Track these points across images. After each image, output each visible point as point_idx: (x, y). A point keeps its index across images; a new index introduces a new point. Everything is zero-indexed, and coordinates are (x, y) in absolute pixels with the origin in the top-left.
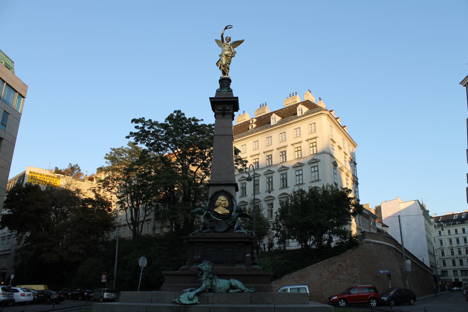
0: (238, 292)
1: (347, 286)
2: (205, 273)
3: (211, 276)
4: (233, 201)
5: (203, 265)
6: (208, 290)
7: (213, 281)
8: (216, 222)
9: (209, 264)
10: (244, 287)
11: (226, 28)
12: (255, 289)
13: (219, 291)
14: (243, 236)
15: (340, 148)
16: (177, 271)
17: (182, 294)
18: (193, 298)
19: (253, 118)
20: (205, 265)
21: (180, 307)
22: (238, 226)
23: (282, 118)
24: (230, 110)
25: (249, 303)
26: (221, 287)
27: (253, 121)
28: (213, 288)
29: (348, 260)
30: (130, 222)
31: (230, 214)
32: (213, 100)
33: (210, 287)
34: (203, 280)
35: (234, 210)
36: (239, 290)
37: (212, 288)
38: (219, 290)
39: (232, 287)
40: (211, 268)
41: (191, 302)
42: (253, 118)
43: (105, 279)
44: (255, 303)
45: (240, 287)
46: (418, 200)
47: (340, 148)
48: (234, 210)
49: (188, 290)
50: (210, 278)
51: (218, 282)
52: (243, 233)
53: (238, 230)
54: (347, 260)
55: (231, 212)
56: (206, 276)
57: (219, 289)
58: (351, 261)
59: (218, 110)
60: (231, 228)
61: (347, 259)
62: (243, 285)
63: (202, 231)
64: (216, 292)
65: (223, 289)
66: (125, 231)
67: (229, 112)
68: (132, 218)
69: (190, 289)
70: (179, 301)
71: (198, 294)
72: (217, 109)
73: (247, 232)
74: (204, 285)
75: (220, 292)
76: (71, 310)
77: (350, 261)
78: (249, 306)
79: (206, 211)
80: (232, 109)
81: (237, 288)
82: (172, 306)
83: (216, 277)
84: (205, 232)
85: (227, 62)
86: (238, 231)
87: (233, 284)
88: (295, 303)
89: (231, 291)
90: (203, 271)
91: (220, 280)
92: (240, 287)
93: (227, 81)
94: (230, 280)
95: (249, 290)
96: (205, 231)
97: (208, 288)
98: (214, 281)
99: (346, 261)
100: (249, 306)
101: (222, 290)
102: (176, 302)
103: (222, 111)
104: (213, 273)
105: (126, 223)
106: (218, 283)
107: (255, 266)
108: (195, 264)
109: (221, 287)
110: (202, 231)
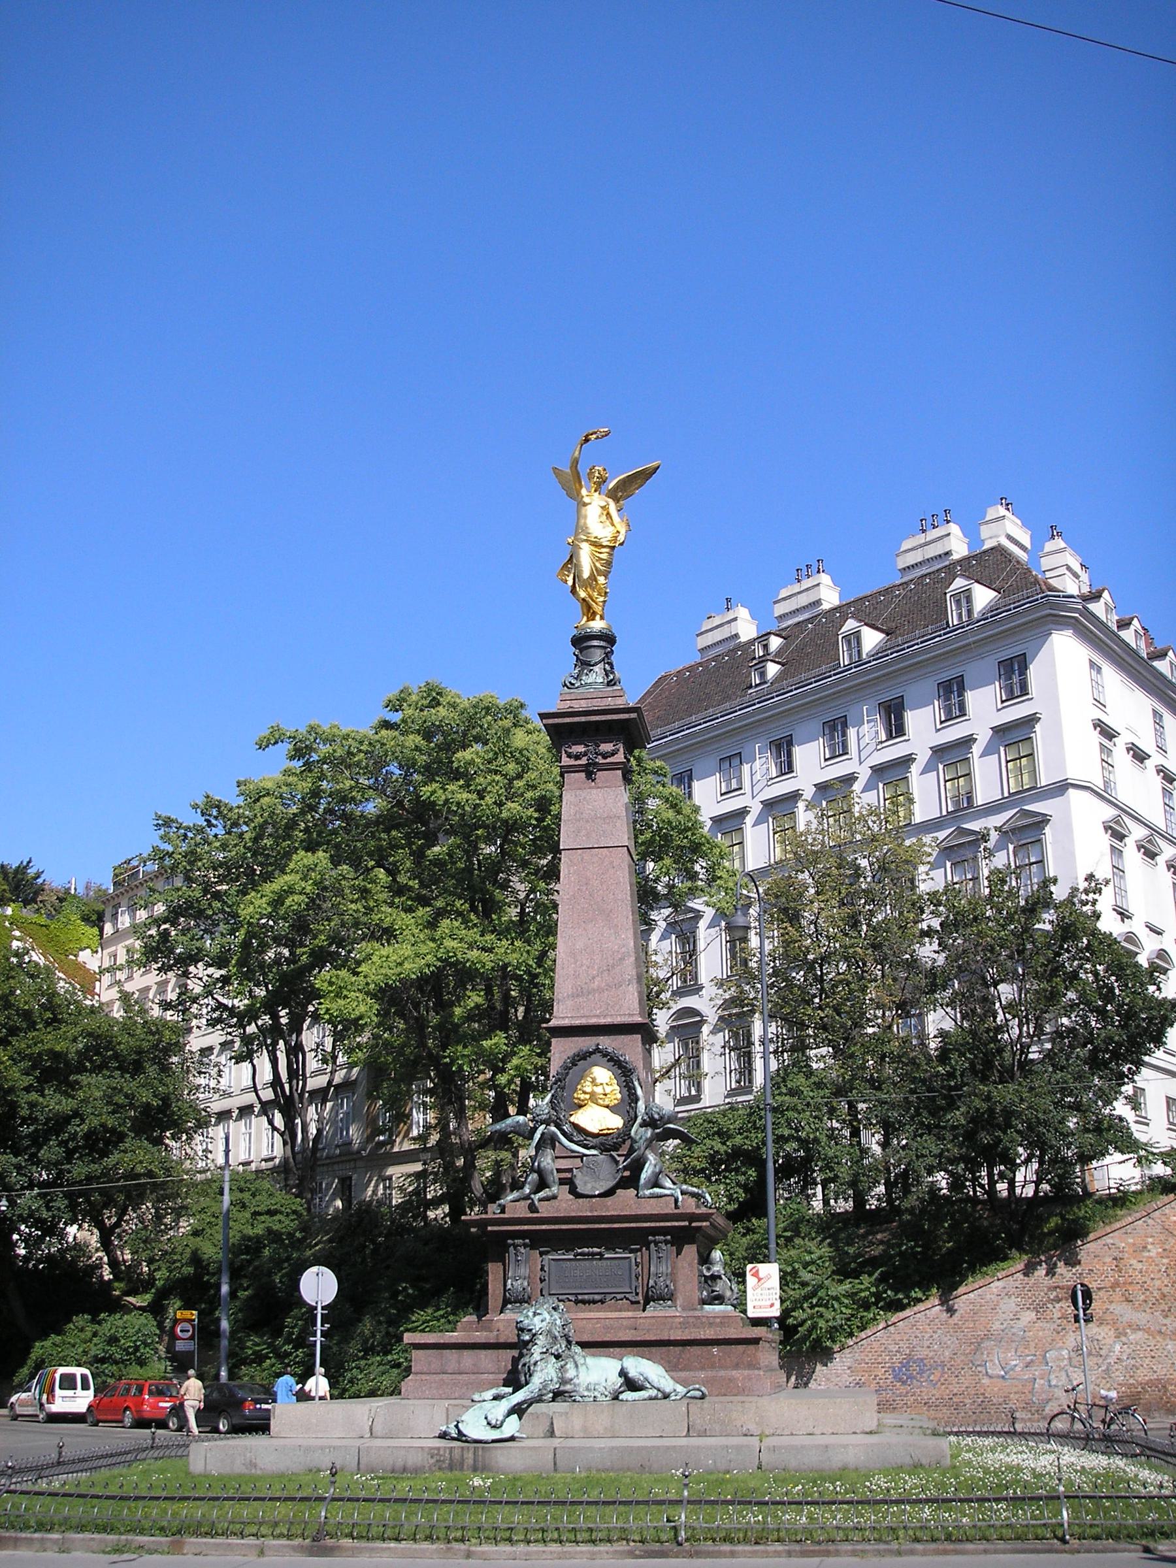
0: (651, 1398)
1: (1149, 1349)
2: (541, 1340)
3: (560, 1347)
4: (636, 1083)
5: (535, 1314)
6: (551, 1395)
7: (568, 1366)
8: (579, 1159)
9: (555, 1309)
10: (671, 1382)
11: (587, 440)
12: (703, 1389)
13: (590, 1397)
14: (670, 1209)
15: (1139, 756)
16: (451, 1334)
17: (467, 1408)
18: (502, 1423)
19: (769, 633)
20: (539, 1314)
21: (462, 1448)
22: (653, 1172)
23: (888, 634)
24: (613, 754)
25: (684, 1434)
26: (595, 1384)
27: (766, 647)
28: (568, 1387)
29: (1153, 1244)
30: (268, 1095)
31: (624, 1134)
32: (550, 721)
33: (557, 1386)
34: (535, 1364)
35: (639, 1120)
36: (653, 1393)
37: (562, 1388)
38: (586, 1393)
39: (632, 1385)
40: (558, 1322)
41: (496, 1434)
42: (769, 633)
43: (192, 1338)
44: (703, 1434)
45: (656, 1380)
46: (501, 1426)
47: (1139, 756)
48: (639, 1120)
49: (489, 1395)
50: (557, 1357)
51: (584, 1367)
52: (668, 1198)
53: (652, 1188)
54: (1149, 1247)
55: (630, 1121)
56: (544, 1350)
57: (588, 1389)
58: (1165, 1250)
59: (569, 756)
60: (630, 1181)
61: (1150, 1240)
62: (667, 1377)
63: (533, 1196)
64: (578, 1398)
65: (602, 1389)
66: (250, 1134)
67: (609, 760)
68: (276, 1083)
69: (494, 1391)
70: (460, 1432)
71: (518, 1410)
72: (566, 752)
73: (683, 1193)
74: (536, 1381)
75: (592, 1399)
76: (104, 1464)
77: (1160, 1250)
78: (684, 1442)
79: (543, 1126)
80: (622, 750)
81: (648, 1386)
82: (438, 1449)
83: (578, 1349)
84: (540, 1200)
85: (595, 566)
86: (651, 1191)
87: (632, 1373)
88: (831, 1431)
89: (628, 1396)
90: (534, 1335)
91: (590, 1361)
92: (656, 1380)
93: (602, 643)
94: (624, 1359)
95: (685, 1390)
96: (541, 1194)
97: (552, 1387)
98: (570, 1366)
99: (1146, 1247)
100: (684, 1442)
101: (596, 1394)
102: (450, 1433)
103: (584, 761)
104: (566, 1337)
105: (251, 1098)
106: (582, 1369)
107: (718, 1308)
108: (509, 1306)
109: (592, 1382)
110: (533, 1196)
